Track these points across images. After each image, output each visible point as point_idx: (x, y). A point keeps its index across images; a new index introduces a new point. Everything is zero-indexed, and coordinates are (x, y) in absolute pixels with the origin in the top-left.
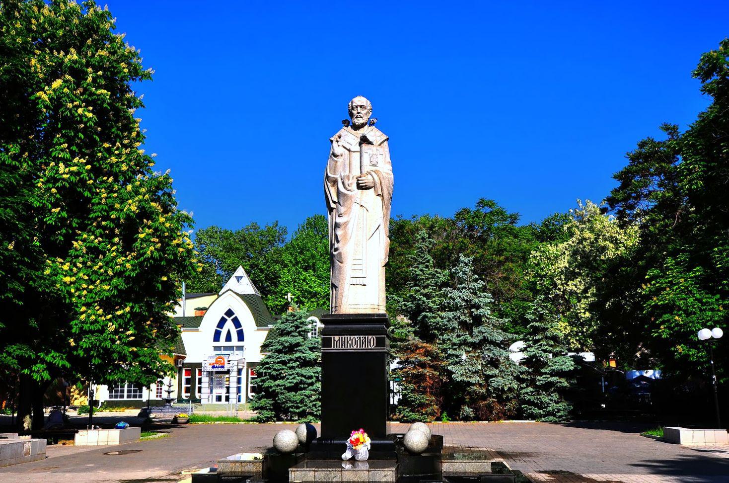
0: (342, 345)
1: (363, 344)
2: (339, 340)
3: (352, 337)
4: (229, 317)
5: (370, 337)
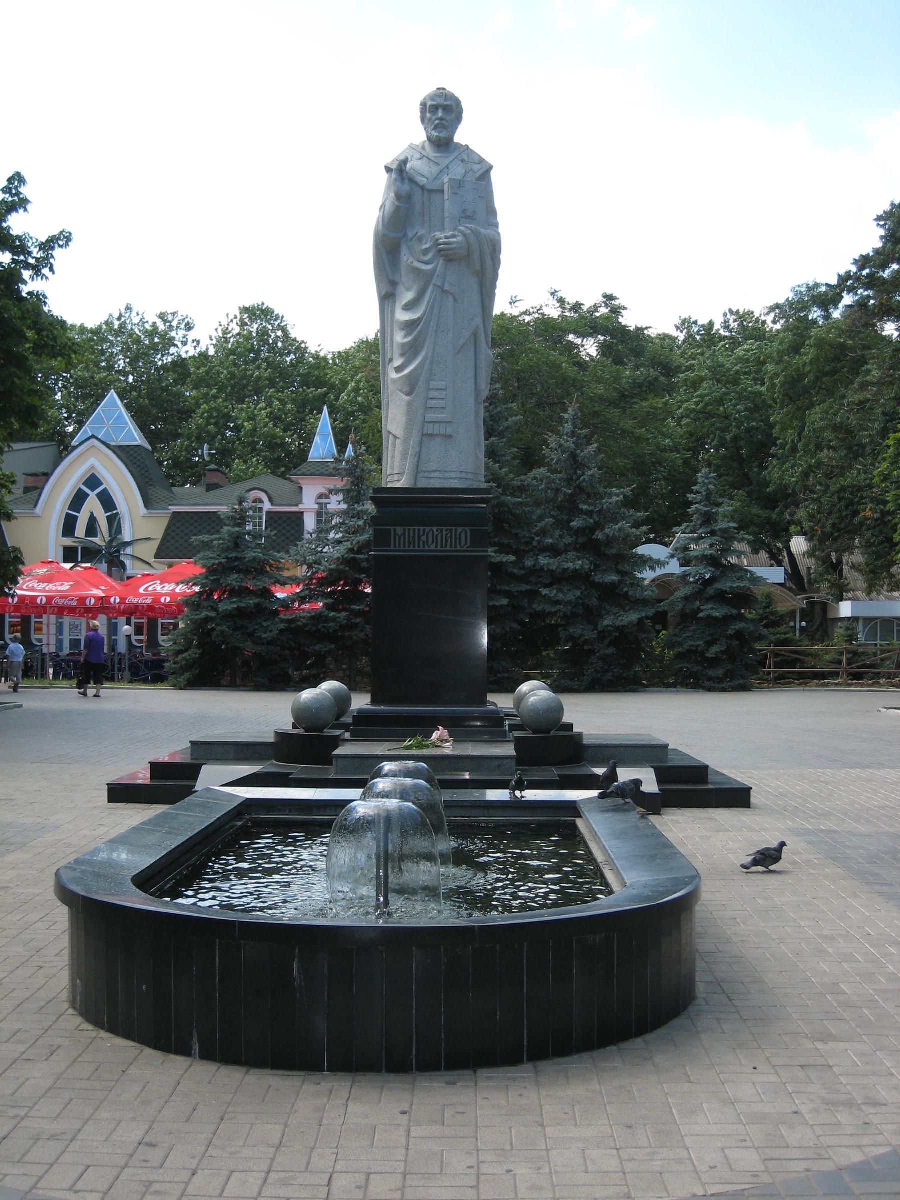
0: (410, 543)
1: (447, 541)
2: (404, 534)
3: (428, 529)
4: (93, 490)
5: (460, 530)
